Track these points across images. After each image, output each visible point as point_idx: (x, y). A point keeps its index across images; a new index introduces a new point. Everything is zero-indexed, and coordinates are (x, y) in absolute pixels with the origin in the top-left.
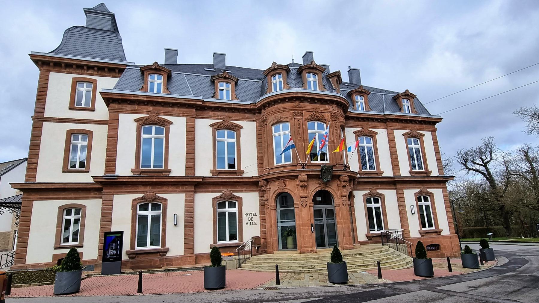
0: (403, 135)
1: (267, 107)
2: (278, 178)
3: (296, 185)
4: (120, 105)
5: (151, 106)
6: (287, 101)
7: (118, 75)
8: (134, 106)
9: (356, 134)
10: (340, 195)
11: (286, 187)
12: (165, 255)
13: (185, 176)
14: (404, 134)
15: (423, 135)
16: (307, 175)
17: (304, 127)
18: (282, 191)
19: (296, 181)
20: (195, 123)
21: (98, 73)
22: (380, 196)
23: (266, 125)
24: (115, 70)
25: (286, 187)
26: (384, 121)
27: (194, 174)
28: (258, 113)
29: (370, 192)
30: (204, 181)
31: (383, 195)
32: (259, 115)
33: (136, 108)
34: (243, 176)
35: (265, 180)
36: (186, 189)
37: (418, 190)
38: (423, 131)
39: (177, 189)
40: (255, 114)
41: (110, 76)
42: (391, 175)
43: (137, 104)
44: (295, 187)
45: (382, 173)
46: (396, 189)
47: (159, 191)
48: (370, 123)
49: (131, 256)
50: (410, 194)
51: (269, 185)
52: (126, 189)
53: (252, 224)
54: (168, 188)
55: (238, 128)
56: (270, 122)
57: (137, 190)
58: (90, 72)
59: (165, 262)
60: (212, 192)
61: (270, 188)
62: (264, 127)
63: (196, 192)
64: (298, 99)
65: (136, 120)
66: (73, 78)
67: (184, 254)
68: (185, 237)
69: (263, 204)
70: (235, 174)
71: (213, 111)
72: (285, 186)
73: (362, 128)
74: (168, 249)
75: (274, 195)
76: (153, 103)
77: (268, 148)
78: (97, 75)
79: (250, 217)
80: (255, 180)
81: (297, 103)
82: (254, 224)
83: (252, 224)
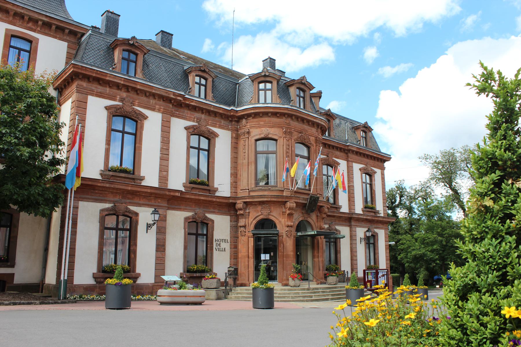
0: (106, 108)
1: (251, 118)
2: (261, 203)
3: (281, 213)
4: (90, 84)
5: (125, 92)
6: (278, 117)
7: (45, 31)
8: (105, 88)
9: (110, 111)
10: (319, 228)
11: (271, 214)
12: (103, 282)
13: (157, 186)
14: (187, 127)
15: (146, 118)
16: (295, 202)
17: (293, 149)
18: (265, 217)
19: (282, 207)
20: (169, 122)
21: (41, 29)
22: (130, 215)
23: (247, 139)
24: (37, 22)
25: (271, 214)
26: (346, 152)
27: (167, 186)
28: (235, 121)
29: (330, 227)
30: (183, 196)
31: (213, 221)
32: (236, 124)
33: (108, 92)
34: (142, 184)
35: (245, 202)
36: (159, 202)
37: (189, 214)
38: (187, 120)
39: (149, 202)
40: (231, 121)
41: (55, 37)
42: (155, 184)
43: (110, 87)
44: (280, 214)
45: (142, 180)
46: (350, 226)
47: (130, 203)
48: (334, 152)
49: (99, 280)
50: (361, 232)
51: (248, 209)
52: (93, 196)
53: (221, 250)
54: (140, 200)
55: (213, 136)
56: (254, 136)
57: (106, 198)
58: (30, 25)
59: (136, 290)
60: (184, 210)
61: (249, 213)
62: (244, 139)
63: (169, 208)
64: (290, 116)
65: (186, 128)
66: (7, 30)
67: (155, 282)
68: (157, 262)
69: (235, 229)
70: (208, 192)
71: (189, 110)
72: (269, 212)
73: (328, 156)
74: (139, 274)
75: (254, 222)
76: (189, 107)
77: (248, 165)
78: (39, 32)
79: (218, 243)
80: (231, 201)
81: (289, 120)
82: (223, 250)
83: (221, 250)
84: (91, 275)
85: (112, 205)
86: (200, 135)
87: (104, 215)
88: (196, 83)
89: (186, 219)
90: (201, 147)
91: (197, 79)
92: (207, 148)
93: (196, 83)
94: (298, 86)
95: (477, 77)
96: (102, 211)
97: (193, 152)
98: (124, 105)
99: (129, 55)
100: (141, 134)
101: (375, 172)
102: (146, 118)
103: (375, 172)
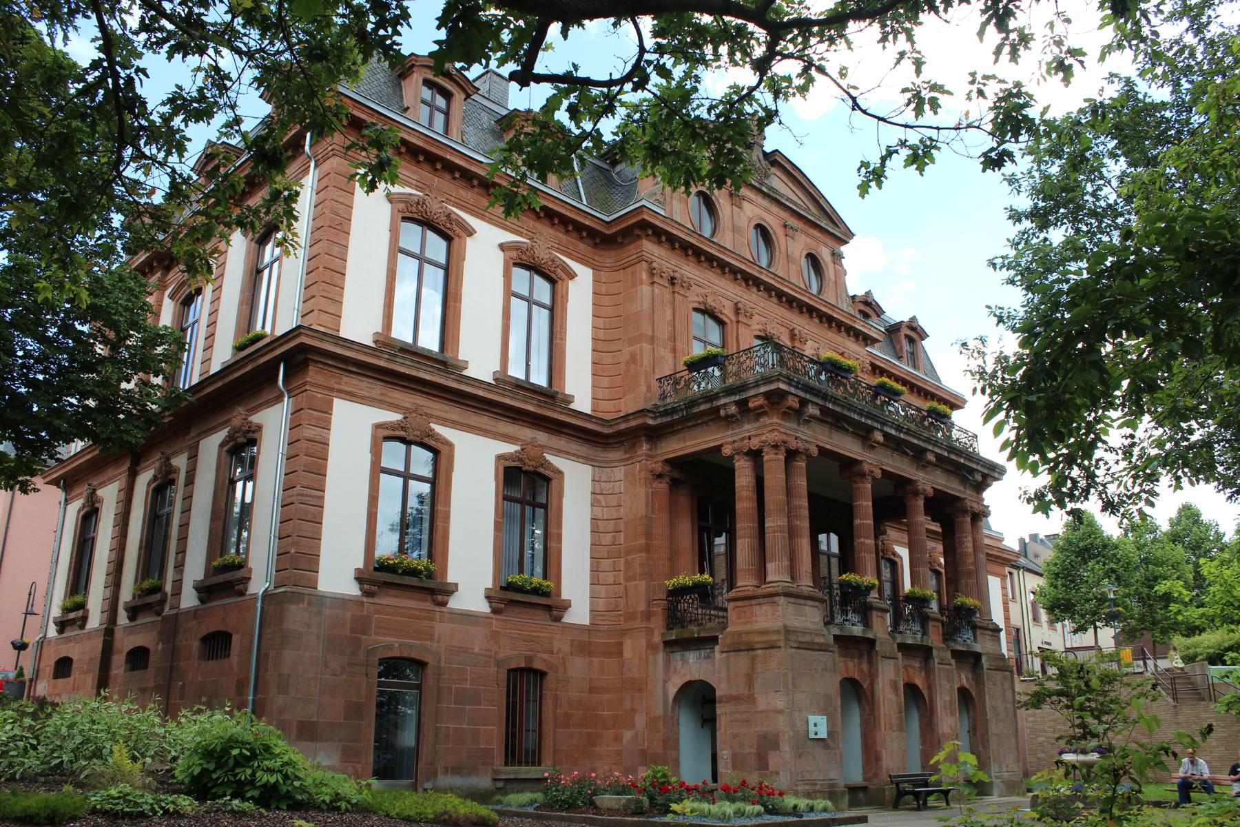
0: (502, 247)
15: (470, 232)
31: (450, 446)
84: (353, 581)
85: (518, 448)
86: (427, 223)
87: (384, 434)
88: (423, 102)
89: (500, 458)
90: (536, 297)
91: (426, 93)
92: (443, 260)
93: (423, 102)
94: (862, 307)
95: (893, 142)
96: (378, 427)
97: (519, 307)
98: (426, 197)
99: (433, 98)
100: (564, 309)
101: (572, 275)
102: (470, 232)
103: (572, 275)
